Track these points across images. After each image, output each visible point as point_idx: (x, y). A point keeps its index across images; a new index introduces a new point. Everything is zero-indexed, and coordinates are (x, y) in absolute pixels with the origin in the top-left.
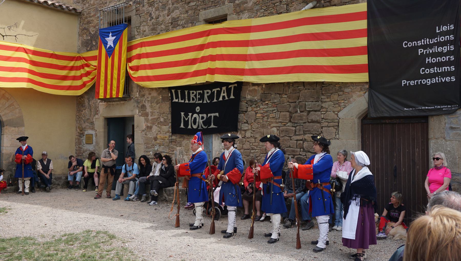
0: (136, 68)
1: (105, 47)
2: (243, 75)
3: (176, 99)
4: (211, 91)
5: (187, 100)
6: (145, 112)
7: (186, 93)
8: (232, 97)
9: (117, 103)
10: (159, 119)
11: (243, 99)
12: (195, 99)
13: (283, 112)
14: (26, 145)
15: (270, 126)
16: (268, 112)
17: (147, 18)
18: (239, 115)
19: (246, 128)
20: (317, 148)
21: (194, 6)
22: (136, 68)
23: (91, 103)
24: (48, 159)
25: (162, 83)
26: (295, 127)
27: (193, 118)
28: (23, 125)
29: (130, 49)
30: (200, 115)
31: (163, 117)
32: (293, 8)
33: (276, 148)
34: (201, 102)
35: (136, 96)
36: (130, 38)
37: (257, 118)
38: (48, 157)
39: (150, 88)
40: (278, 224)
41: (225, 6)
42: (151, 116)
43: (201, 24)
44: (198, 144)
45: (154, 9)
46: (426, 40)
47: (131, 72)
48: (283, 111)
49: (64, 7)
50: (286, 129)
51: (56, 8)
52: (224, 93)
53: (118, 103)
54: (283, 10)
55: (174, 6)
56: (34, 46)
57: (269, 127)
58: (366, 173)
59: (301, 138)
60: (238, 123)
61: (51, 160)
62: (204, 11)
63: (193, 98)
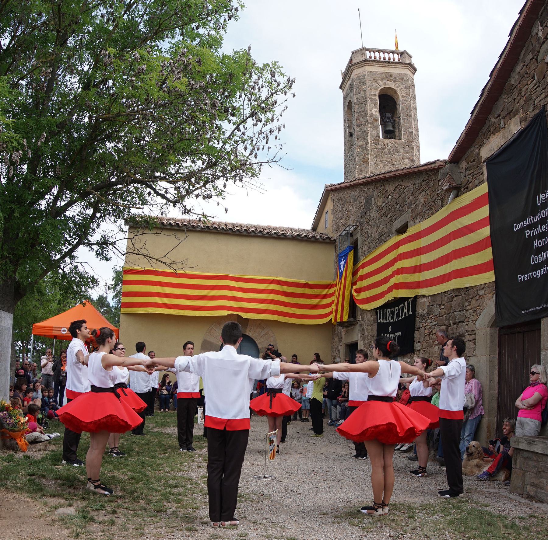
0: (359, 291)
8: (411, 313)
22: (359, 291)
29: (355, 273)
34: (392, 320)
46: (530, 218)
47: (355, 294)
48: (442, 324)
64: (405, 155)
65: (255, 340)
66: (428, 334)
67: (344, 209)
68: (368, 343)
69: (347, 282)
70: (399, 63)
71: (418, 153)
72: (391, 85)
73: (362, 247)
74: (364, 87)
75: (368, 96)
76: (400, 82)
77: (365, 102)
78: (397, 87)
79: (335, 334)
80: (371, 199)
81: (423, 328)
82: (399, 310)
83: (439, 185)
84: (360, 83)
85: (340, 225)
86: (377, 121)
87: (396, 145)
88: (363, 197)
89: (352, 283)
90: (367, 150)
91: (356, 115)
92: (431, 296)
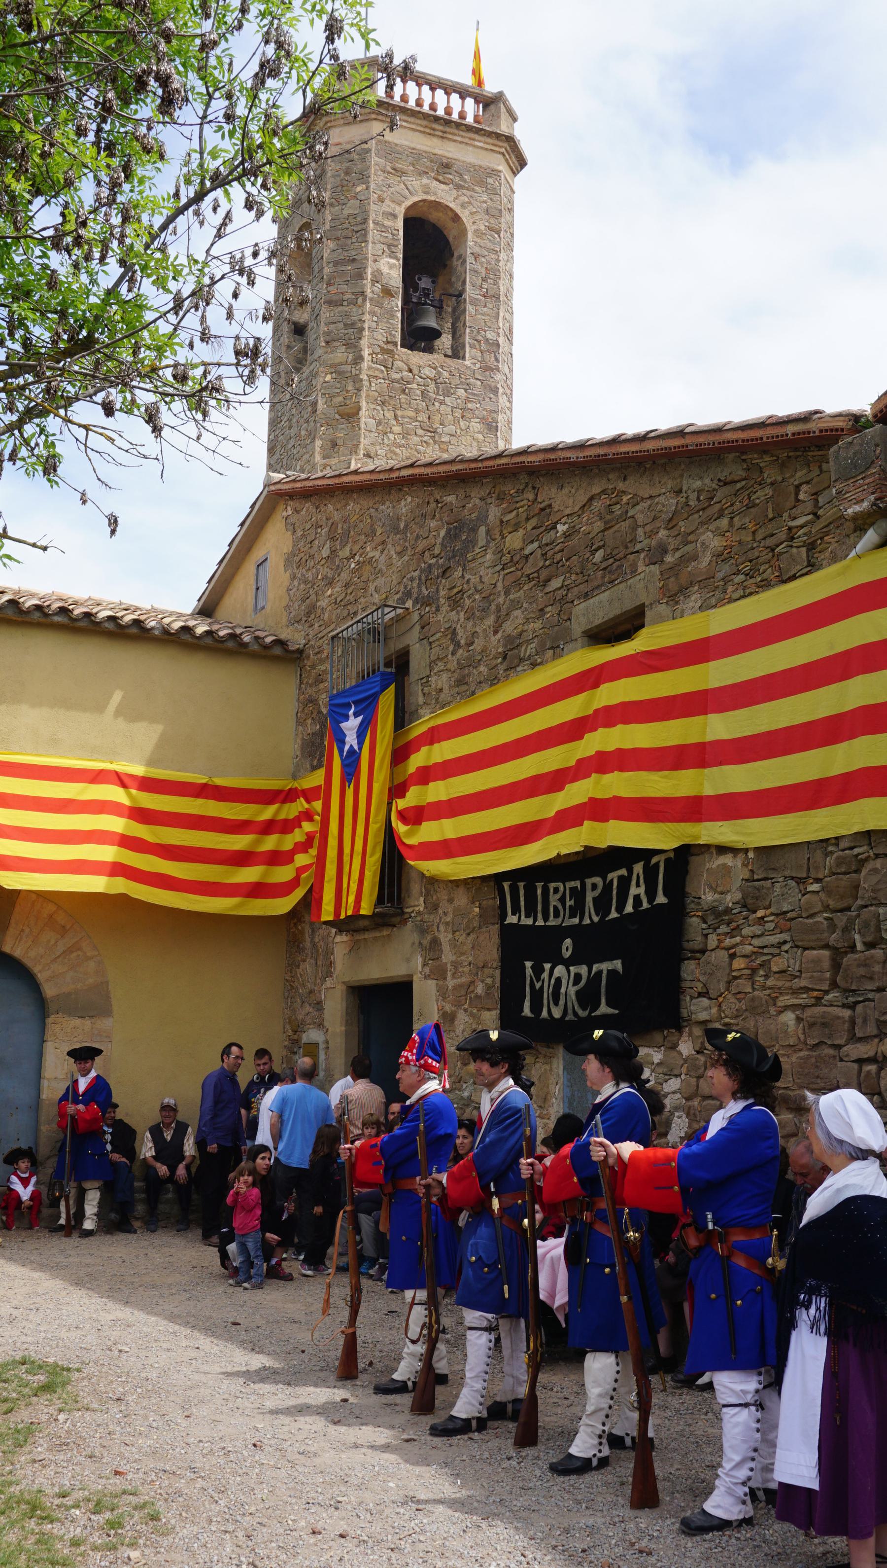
0: (415, 816)
1: (341, 751)
2: (700, 820)
3: (513, 914)
4: (604, 879)
5: (540, 915)
6: (438, 963)
7: (539, 891)
8: (661, 899)
9: (367, 935)
10: (471, 988)
11: (692, 906)
12: (562, 914)
13: (814, 949)
14: (93, 1074)
15: (775, 1004)
16: (766, 951)
17: (447, 648)
18: (683, 967)
19: (704, 1013)
20: (719, 1078)
21: (559, 589)
22: (415, 816)
23: (317, 940)
24: (178, 1122)
25: (478, 863)
26: (852, 1007)
27: (553, 981)
28: (106, 1012)
29: (400, 755)
30: (572, 968)
31: (483, 981)
32: (827, 554)
33: (617, 1084)
34: (576, 921)
35: (417, 909)
36: (401, 721)
37: (734, 974)
38: (180, 1117)
39: (451, 881)
40: (600, 1395)
41: (638, 577)
42: (454, 976)
43: (576, 649)
44: (421, 1066)
45: (462, 614)
47: (401, 828)
48: (812, 944)
49: (247, 638)
50: (823, 1017)
51: (220, 645)
52: (638, 885)
53: (377, 934)
54: (799, 567)
55: (512, 597)
56: (149, 763)
57: (773, 1010)
58: (846, 1186)
59: (871, 1054)
60: (682, 997)
61: (187, 1126)
62: (584, 604)
63: (555, 907)
64: (470, 405)
65: (36, 970)
66: (748, 972)
67: (346, 552)
68: (456, 988)
69: (376, 786)
70: (478, 131)
71: (508, 404)
72: (445, 194)
73: (425, 681)
74: (359, 189)
75: (372, 216)
76: (474, 191)
77: (362, 234)
78: (463, 206)
79: (301, 950)
80: (474, 530)
81: (723, 955)
82: (608, 887)
83: (798, 500)
84: (347, 173)
85: (323, 603)
86: (392, 296)
87: (445, 374)
88: (433, 524)
89: (390, 789)
90: (357, 380)
91: (327, 270)
92: (756, 849)
